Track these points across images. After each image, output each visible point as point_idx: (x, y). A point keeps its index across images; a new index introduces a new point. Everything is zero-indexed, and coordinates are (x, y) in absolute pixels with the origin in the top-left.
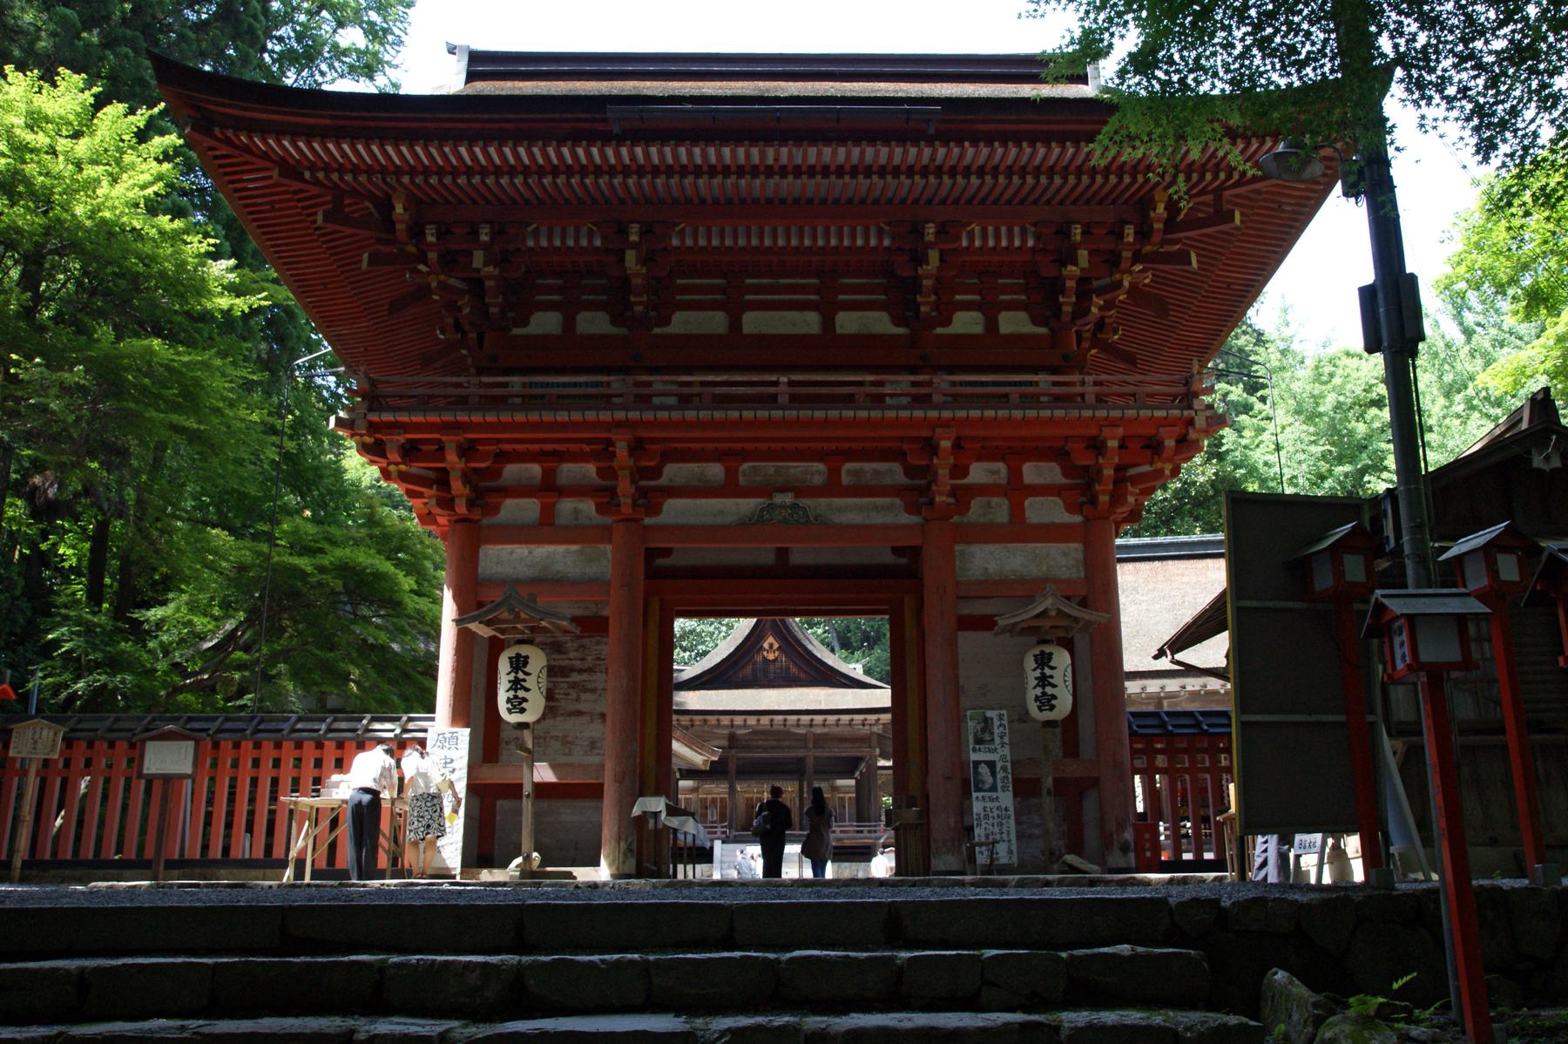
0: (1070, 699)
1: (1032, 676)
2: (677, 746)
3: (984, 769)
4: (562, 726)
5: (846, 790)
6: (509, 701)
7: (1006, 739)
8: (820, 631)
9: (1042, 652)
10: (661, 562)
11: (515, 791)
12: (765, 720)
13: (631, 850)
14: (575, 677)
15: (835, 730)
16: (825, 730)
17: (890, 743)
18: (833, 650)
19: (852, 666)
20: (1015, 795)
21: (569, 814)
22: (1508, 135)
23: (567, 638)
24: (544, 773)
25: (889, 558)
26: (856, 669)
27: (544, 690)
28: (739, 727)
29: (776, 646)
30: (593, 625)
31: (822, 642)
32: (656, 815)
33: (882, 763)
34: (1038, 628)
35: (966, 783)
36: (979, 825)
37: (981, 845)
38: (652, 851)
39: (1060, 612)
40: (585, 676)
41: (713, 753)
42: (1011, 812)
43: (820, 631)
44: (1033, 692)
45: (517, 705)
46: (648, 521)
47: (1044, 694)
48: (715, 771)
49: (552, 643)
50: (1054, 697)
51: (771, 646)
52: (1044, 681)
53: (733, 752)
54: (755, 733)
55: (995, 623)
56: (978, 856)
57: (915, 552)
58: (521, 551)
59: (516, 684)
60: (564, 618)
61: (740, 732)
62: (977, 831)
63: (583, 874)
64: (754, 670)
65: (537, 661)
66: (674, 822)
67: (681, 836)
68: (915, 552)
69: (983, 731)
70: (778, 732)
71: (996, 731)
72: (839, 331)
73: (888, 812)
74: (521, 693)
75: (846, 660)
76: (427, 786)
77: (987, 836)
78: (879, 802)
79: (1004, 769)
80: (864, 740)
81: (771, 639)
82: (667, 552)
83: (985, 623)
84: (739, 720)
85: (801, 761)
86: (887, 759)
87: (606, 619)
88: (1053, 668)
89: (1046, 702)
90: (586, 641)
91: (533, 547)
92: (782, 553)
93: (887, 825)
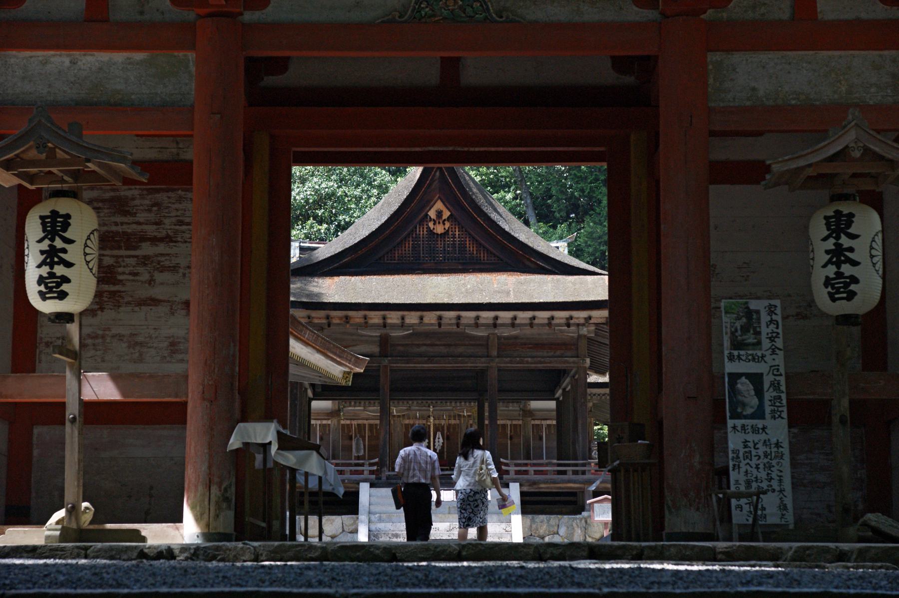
0: (880, 281)
1: (821, 249)
2: (296, 348)
3: (745, 386)
4: (128, 320)
5: (544, 414)
6: (41, 280)
7: (779, 343)
8: (509, 196)
9: (838, 213)
10: (270, 81)
11: (55, 412)
12: (430, 317)
13: (226, 499)
14: (147, 249)
15: (528, 331)
16: (515, 332)
17: (607, 351)
18: (527, 223)
19: (554, 244)
20: (790, 426)
21: (139, 445)
22: (503, 577)
23: (134, 192)
24: (101, 387)
25: (606, 75)
26: (559, 249)
27: (94, 264)
28: (393, 326)
29: (446, 214)
30: (169, 174)
31: (512, 210)
32: (266, 447)
33: (593, 378)
34: (833, 176)
35: (718, 406)
36: (737, 467)
37: (739, 496)
38: (256, 504)
39: (867, 150)
40: (161, 248)
41: (357, 362)
42: (786, 450)
43: (509, 196)
44: (821, 272)
45: (54, 287)
46: (248, 17)
47: (839, 275)
48: (359, 388)
49: (111, 200)
50: (854, 280)
51: (439, 214)
52: (839, 255)
53: (386, 361)
54: (416, 335)
55: (768, 169)
56: (735, 512)
57: (645, 65)
58: (59, 60)
59: (51, 257)
60: (123, 159)
61: (395, 334)
62: (733, 475)
63: (156, 534)
64: (415, 248)
65: (83, 222)
66: (290, 459)
67: (300, 479)
68: (645, 65)
69: (745, 329)
70: (449, 334)
71: (765, 330)
72: (607, 298)
73: (602, 446)
74: (59, 270)
75: (547, 236)
76: (533, 518)
77: (748, 483)
78: (589, 432)
79: (775, 385)
80: (569, 346)
81: (439, 205)
82: (280, 65)
83: (752, 172)
84: (394, 317)
85: (481, 374)
86: (602, 373)
87: (190, 163)
88: (853, 237)
89: (842, 287)
90: (162, 197)
91: (76, 53)
92: (451, 66)
93: (601, 464)
